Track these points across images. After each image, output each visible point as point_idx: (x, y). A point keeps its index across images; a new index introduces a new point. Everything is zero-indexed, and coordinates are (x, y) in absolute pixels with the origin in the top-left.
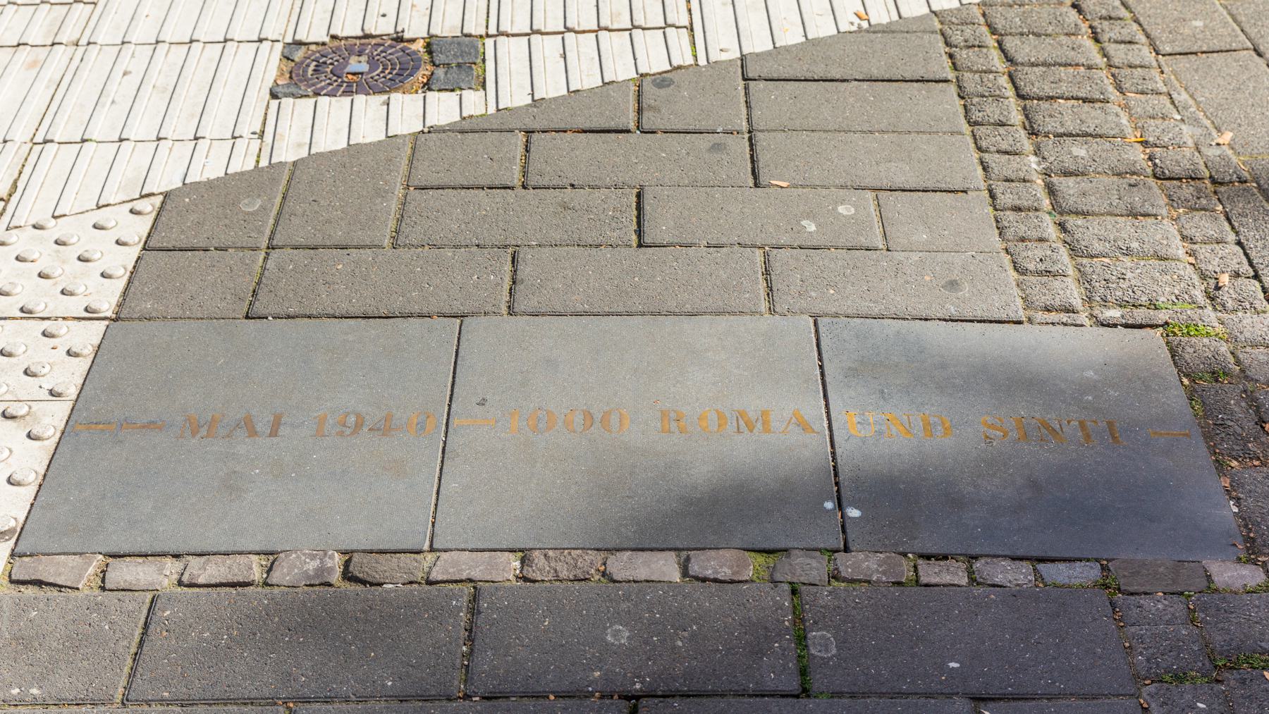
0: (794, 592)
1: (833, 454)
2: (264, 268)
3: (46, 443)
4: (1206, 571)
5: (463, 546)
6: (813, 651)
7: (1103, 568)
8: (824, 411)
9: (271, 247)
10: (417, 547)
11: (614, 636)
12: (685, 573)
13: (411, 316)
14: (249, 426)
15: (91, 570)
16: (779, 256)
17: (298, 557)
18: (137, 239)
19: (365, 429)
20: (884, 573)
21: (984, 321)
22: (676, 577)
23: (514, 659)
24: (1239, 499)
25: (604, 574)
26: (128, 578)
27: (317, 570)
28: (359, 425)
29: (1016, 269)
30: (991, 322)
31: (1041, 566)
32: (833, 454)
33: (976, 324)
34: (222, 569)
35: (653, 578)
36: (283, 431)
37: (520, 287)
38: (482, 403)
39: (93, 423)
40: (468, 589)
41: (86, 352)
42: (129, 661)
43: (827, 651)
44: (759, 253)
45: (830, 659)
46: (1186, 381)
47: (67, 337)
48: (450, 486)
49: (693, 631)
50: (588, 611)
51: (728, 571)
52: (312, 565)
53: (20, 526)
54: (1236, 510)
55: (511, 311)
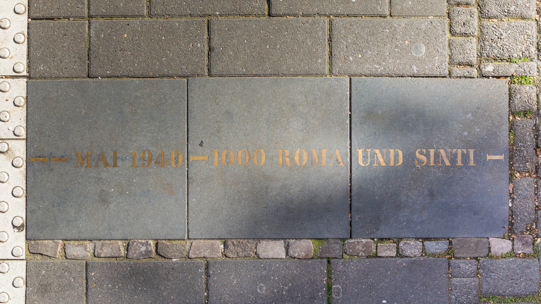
0: (329, 262)
1: (351, 190)
2: (89, 34)
3: (21, 168)
4: (489, 244)
5: (200, 237)
6: (333, 296)
7: (450, 243)
8: (349, 150)
9: (90, 16)
10: (182, 238)
11: (260, 289)
12: (287, 254)
13: (163, 76)
14: (102, 157)
15: (59, 248)
16: (337, 21)
17: (137, 244)
18: (23, 9)
19: (153, 162)
20: (364, 252)
21: (429, 77)
22: (283, 256)
23: (224, 301)
24: (514, 199)
25: (256, 254)
26: (75, 253)
27: (145, 251)
28: (150, 160)
29: (450, 32)
30: (431, 77)
31: (426, 243)
32: (351, 176)
33: (425, 78)
34: (109, 250)
35: (275, 257)
36: (119, 163)
37: (213, 54)
38: (201, 144)
39: (33, 228)
40: (204, 262)
41: (22, 104)
42: (85, 297)
43: (339, 295)
44: (327, 20)
45: (339, 299)
46: (511, 118)
47: (10, 91)
48: (193, 201)
49: (290, 286)
50: (250, 275)
51: (304, 254)
52: (143, 249)
53: (25, 221)
54: (510, 205)
55: (210, 75)
